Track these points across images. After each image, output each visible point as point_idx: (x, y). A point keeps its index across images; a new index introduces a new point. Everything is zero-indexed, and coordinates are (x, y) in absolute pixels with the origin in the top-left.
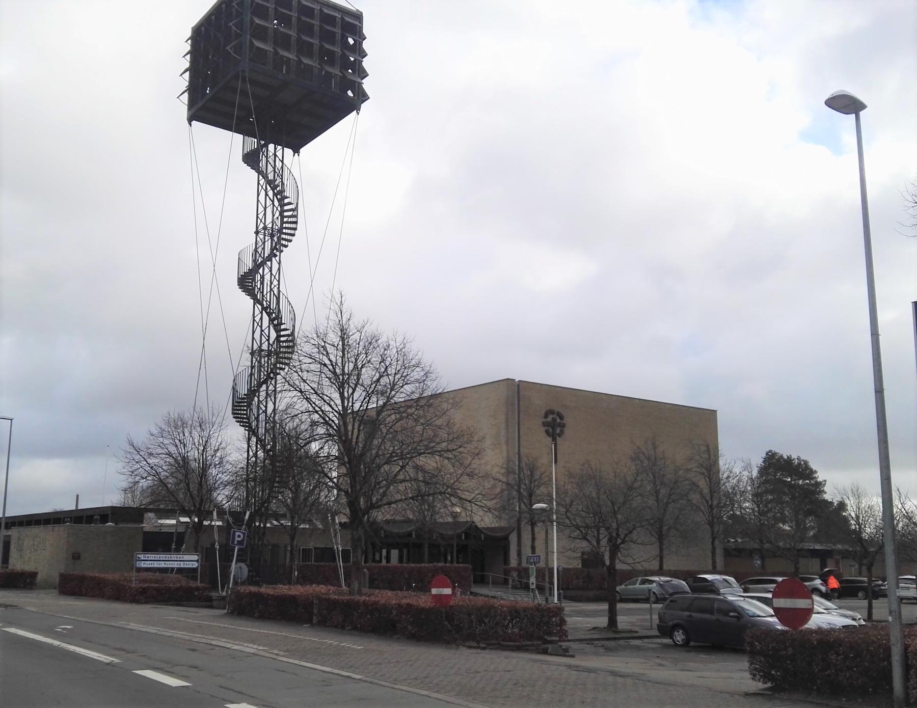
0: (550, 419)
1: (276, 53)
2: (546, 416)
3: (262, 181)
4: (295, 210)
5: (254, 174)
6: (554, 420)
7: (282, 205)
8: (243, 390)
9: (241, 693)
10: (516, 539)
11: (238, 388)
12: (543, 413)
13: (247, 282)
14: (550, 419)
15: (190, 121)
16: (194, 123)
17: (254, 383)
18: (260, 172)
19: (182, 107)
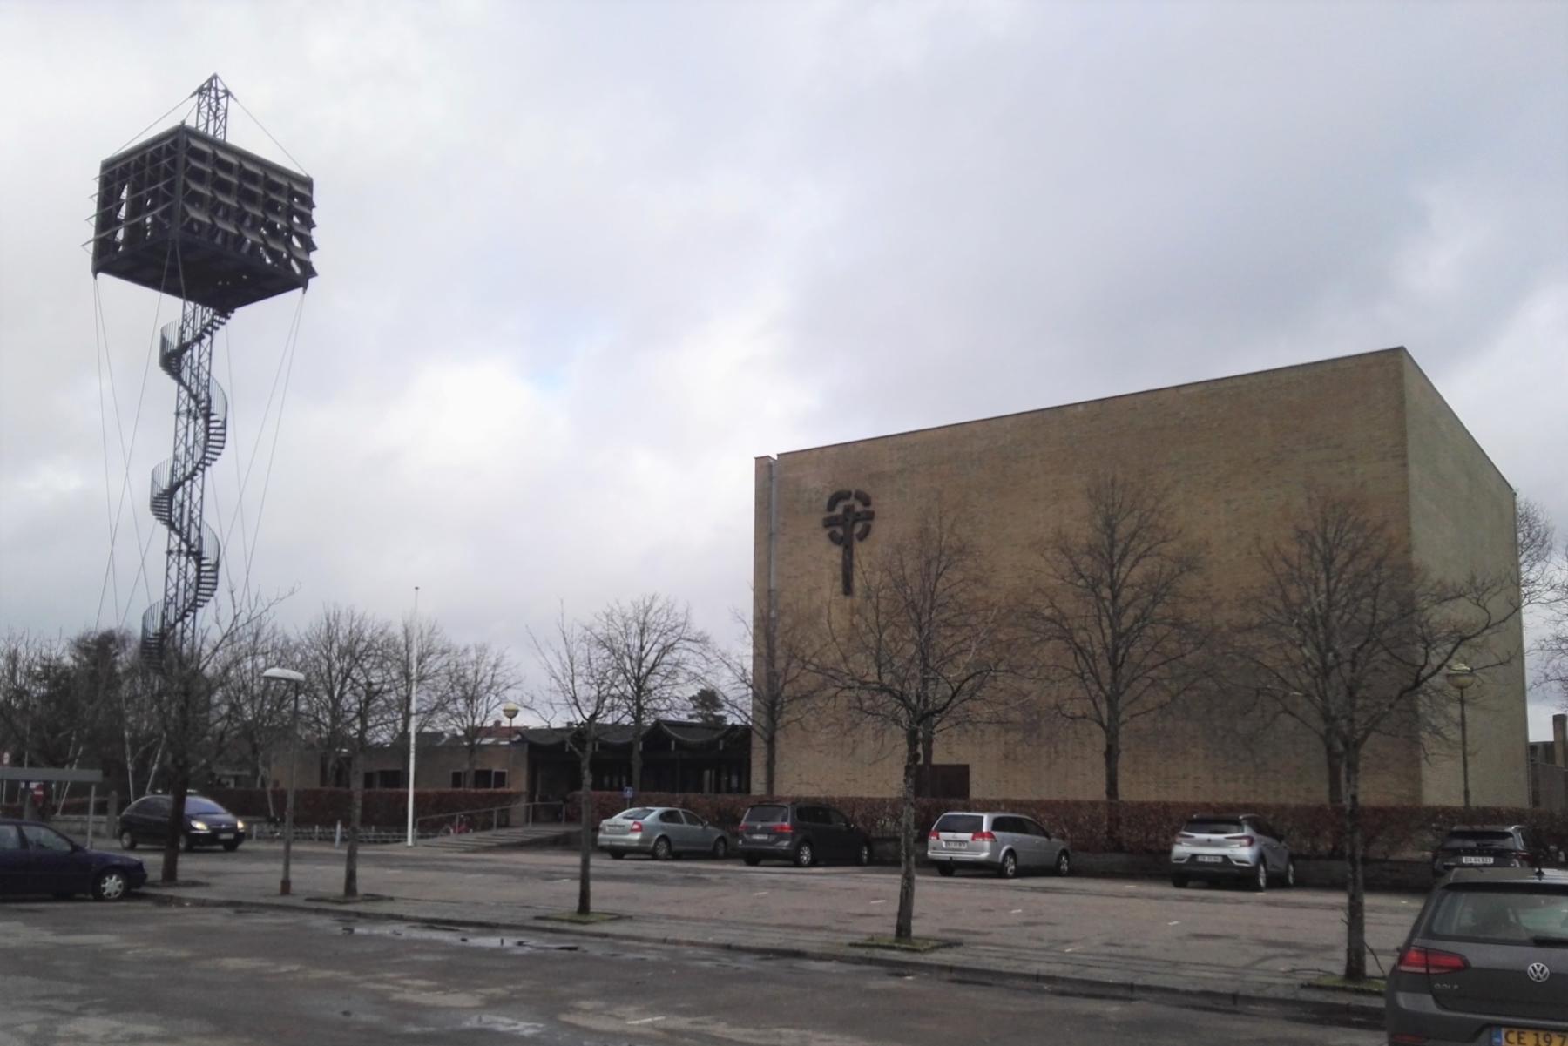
0: (839, 511)
1: (214, 173)
2: (832, 505)
3: (184, 394)
4: (224, 427)
5: (174, 383)
6: (848, 510)
7: (208, 421)
8: (164, 484)
9: (868, 915)
10: (517, 839)
11: (158, 479)
12: (826, 501)
13: (172, 361)
14: (839, 511)
15: (96, 271)
16: (101, 275)
17: (206, 342)
18: (181, 382)
19: (87, 257)
